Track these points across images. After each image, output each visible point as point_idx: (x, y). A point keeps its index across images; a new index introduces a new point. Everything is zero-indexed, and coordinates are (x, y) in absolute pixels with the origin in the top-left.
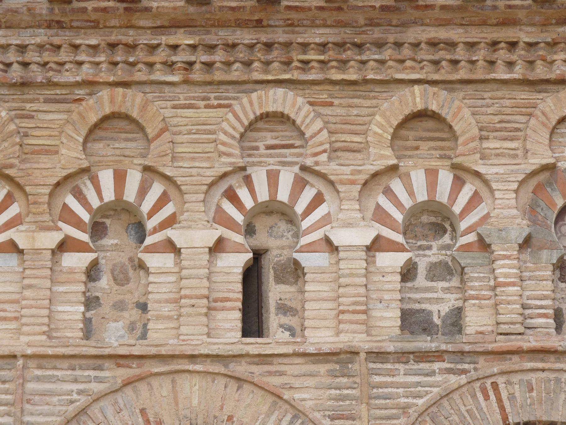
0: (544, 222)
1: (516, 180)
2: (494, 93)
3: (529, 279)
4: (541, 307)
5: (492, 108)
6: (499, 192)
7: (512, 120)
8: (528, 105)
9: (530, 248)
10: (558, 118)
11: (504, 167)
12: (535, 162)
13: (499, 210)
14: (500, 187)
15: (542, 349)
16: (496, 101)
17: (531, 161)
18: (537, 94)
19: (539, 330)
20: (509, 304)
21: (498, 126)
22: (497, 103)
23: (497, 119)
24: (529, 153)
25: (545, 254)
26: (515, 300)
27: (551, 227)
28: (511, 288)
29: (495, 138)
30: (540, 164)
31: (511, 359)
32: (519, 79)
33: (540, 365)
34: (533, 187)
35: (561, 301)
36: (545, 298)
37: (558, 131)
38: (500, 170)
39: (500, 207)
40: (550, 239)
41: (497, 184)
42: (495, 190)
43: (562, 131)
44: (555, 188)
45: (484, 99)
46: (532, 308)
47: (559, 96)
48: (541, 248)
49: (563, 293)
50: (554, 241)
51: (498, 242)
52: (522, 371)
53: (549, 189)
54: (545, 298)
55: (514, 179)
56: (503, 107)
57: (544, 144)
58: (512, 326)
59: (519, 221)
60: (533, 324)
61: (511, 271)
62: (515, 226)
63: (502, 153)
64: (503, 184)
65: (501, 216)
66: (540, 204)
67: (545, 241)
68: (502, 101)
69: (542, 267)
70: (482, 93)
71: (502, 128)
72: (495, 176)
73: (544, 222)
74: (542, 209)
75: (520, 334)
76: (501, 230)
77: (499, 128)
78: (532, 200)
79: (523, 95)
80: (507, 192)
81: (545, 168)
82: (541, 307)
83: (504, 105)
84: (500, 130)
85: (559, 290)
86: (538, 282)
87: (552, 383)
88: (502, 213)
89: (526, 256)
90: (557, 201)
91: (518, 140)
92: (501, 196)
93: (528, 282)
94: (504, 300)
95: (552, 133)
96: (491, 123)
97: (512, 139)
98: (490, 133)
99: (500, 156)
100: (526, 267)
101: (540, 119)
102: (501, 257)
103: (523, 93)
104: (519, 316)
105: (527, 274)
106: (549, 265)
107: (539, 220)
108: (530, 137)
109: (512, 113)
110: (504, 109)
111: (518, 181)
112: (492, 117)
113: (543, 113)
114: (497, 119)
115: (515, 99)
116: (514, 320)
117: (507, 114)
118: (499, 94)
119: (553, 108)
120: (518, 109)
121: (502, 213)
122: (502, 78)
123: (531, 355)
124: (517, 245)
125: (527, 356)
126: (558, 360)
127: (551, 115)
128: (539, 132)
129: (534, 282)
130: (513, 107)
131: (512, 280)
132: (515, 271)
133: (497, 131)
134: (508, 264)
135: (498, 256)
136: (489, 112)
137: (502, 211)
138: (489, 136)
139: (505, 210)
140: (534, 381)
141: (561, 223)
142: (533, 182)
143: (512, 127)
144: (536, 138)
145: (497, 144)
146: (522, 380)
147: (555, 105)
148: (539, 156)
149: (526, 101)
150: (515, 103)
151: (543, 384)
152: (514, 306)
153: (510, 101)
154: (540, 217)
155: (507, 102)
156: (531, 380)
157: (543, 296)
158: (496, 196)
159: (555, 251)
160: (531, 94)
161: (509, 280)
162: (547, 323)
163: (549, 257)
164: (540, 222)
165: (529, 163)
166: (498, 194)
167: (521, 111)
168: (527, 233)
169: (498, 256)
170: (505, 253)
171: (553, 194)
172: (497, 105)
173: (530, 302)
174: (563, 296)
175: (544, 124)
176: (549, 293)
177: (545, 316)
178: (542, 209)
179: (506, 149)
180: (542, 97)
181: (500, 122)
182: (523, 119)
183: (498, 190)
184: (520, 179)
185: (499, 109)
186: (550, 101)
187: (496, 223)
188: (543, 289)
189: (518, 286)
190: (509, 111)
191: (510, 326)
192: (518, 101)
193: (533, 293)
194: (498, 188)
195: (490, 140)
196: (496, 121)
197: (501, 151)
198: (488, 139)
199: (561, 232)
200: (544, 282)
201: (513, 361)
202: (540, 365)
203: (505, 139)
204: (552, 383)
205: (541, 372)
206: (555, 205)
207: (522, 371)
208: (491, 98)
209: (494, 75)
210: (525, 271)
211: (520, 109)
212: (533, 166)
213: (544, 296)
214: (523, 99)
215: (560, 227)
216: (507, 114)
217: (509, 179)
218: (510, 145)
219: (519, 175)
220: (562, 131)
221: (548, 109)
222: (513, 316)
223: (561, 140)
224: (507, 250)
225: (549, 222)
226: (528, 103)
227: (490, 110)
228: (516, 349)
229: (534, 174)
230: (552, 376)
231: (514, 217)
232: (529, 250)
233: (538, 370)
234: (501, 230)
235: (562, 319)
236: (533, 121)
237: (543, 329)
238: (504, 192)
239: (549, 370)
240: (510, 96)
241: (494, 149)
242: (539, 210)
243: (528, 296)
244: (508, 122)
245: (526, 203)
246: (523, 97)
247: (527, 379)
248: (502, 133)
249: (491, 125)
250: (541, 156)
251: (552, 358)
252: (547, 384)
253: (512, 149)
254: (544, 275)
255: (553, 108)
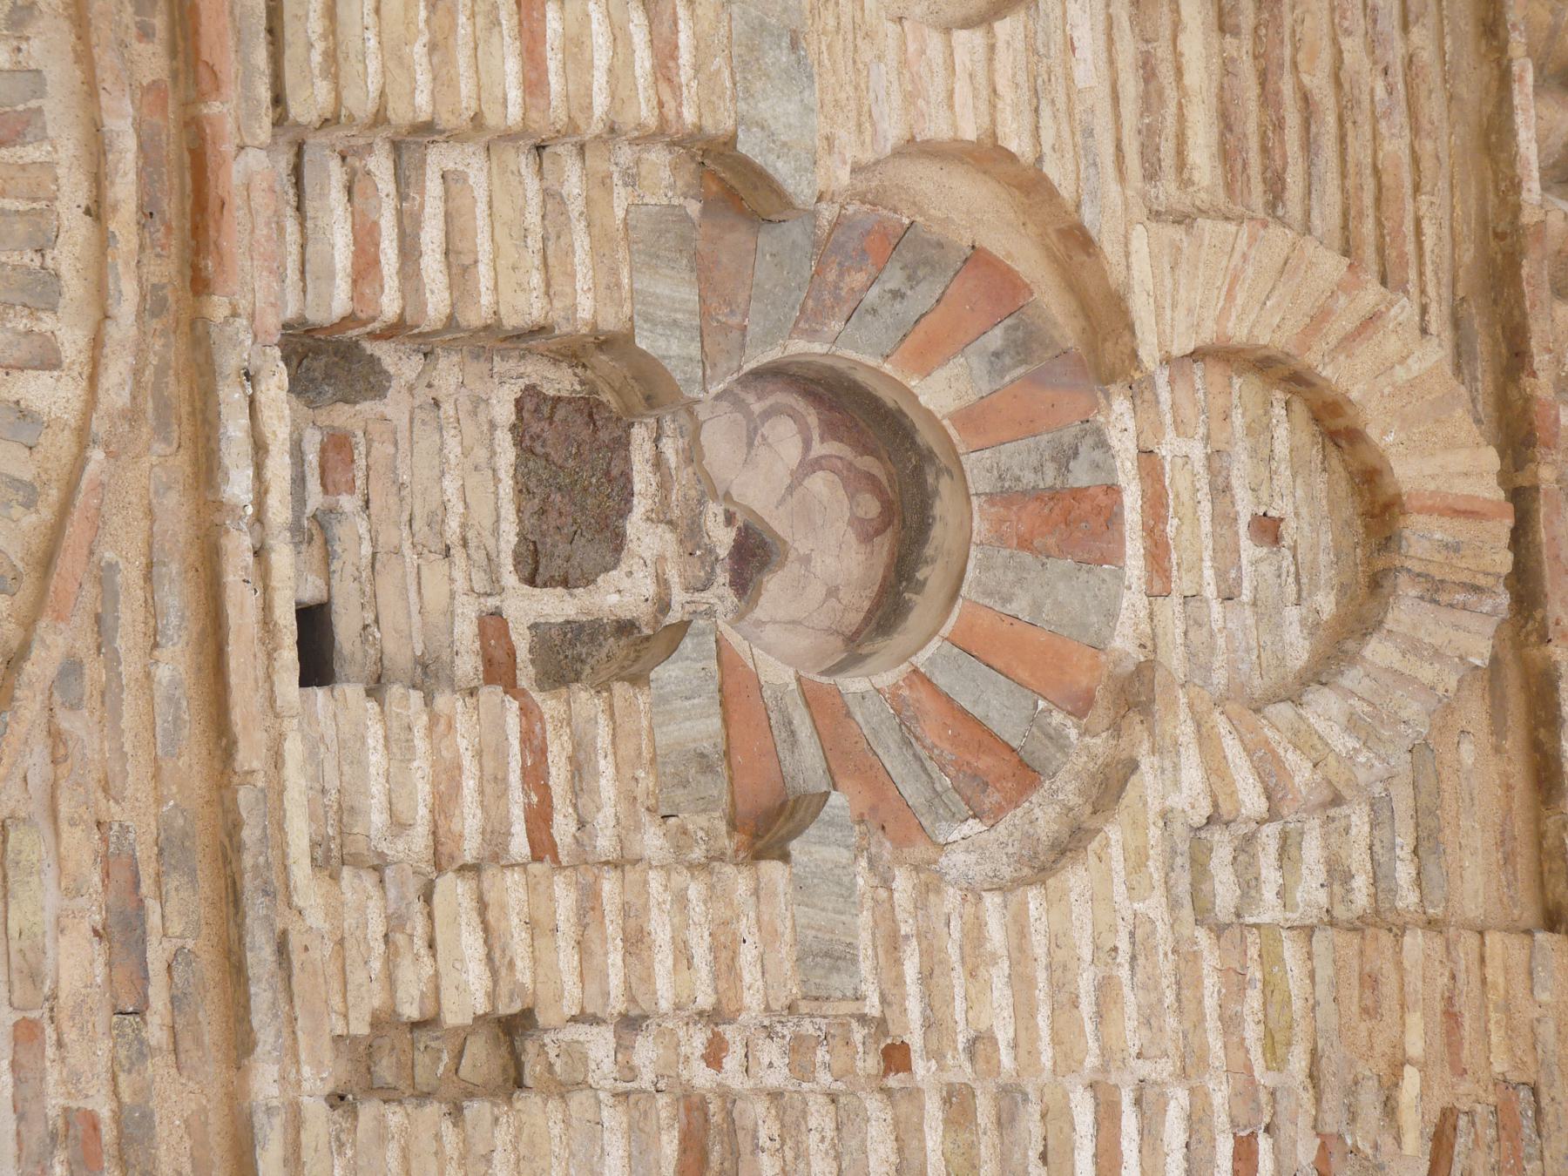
0: (838, 300)
1: (1046, 149)
2: (1434, 75)
3: (547, 194)
4: (409, 250)
5: (1367, 64)
6: (981, 52)
7: (1321, 163)
8: (1392, 254)
9: (704, 212)
10: (1354, 395)
11: (1104, 91)
12: (1137, 259)
13: (892, 43)
14: (1004, 59)
15: (213, 205)
16: (1400, 86)
17: (1140, 240)
18: (1446, 309)
19: (291, 227)
20: (432, 47)
21: (1287, 87)
22: (1390, 91)
23: (1318, 82)
24: (1177, 233)
25: (675, 291)
26: (453, 85)
27: (812, 334)
28: (512, 67)
29: (1228, 68)
30: (1128, 286)
31: (145, 33)
32: (1517, 209)
33: (124, 190)
34: (1000, 255)
35: (423, 395)
36: (459, 270)
37: (1279, 411)
38: (1087, 70)
39: (912, 47)
40: (753, 330)
41: (1019, 45)
42: (990, 32)
43: (1281, 433)
44: (1002, 372)
45: (1405, 27)
46: (402, 196)
47: (1459, 412)
48: (703, 270)
49: (466, 405)
50: (743, 347)
51: (739, 26)
52: (91, 89)
53: (995, 338)
54: (459, 270)
55: (1047, 136)
56: (1375, 121)
57: (1224, 314)
58: (316, 57)
59: (852, 149)
60: (323, 195)
61: (600, 79)
62: (820, 124)
63: (1160, 93)
64: (1022, 78)
65: (867, 53)
66: (924, 287)
67: (741, 298)
68: (1400, 117)
69: (614, 271)
70: (1431, 19)
71: (1279, 105)
72: (1058, 37)
73: (838, 300)
74: (897, 295)
75: (278, 100)
76: (794, 45)
77: (1278, 93)
78: (940, 245)
79: (1438, 225)
80: (985, 93)
81: (1106, 315)
82: (409, 250)
83: (1383, 125)
84: (1268, 97)
85: (478, 388)
86: (534, 243)
87: (30, 259)
88: (880, 58)
89: (663, 180)
90: (941, 375)
91: (1229, 187)
92: (961, 57)
93: (532, 186)
94: (453, 27)
95: (1265, 365)
96: (1296, 50)
97: (1227, 155)
98: (1247, 44)
99: (1147, 81)
100: (605, 182)
101: (1343, 300)
102: (665, 30)
103: (1446, 231)
104: (371, 107)
105: (573, 183)
106: (627, 309)
107: (841, 275)
108: (1253, 239)
109: (1351, 169)
110: (1367, 129)
111: (1040, 159)
112: (1326, 57)
113: (1371, 321)
114: (1318, 82)
115: (1417, 189)
116: (350, 69)
117: (1342, 139)
118: (1433, 108)
119: (1401, 374)
120: (1368, 199)
121: (880, 58)
122: (1519, 119)
123: (172, 146)
124: (729, 124)
125: (168, 124)
126: (152, 304)
127: (1365, 356)
128: (1280, 290)
129: (533, 218)
130: (1376, 172)
131: (555, 82)
132: (600, 102)
133: (1263, 78)
134: (629, 64)
135: (667, 17)
136: (1346, 43)
137: (892, 56)
138: (1236, 32)
139: (893, 76)
140: (32, 153)
141: (813, 419)
142: (1026, 257)
143: (1284, 156)
144: (1250, 270)
145: (1198, 76)
146: (39, 91)
147: (1412, 384)
148: (1168, 283)
149: (1410, 248)
150: (1400, 186)
151: (23, 206)
152: (423, 78)
153: (1406, 159)
154: (858, 279)
155: (1396, 146)
156: (42, 138)
157: (466, 260)
158: (961, 36)
159: (694, 350)
160: (1446, 278)
161: (553, 65)
162: (332, 276)
163: (661, 314)
164: (831, 276)
165: (1129, 224)
166: (968, 42)
167: (1361, 214)
168: (790, 186)
169: (667, 17)
170: (685, 57)
171: (974, 361)
172: (1380, 92)
173: (434, 187)
174: (448, 408)
175: (1320, 318)
176: (486, 299)
177: (365, 267)
178: (897, 295)
179: (1181, 118)
180: (1433, 328)
181: (1306, 98)
182: (1327, 216)
183: (992, 48)
184: (1051, 170)
185: (1366, 98)
186: (1428, 364)
187: (832, 23)
188: (502, 263)
189: (526, 108)
190: (1359, 150)
191: (320, 46)
192: (1410, 207)
193: (481, 208)
194: (1001, 45)
195: (1215, 37)
196: (1306, 79)
197: (1171, 94)
198: (1222, 29)
199: (767, 414)
200: (536, 279)
201: (138, 46)
202: (124, 190)
203: (1226, 120)
204: (30, 259)
205: (83, 197)
206: (925, 362)
207: (91, 89)
208: (1410, 60)
209: (1530, 78)
210: (586, 174)
211: (1370, 212)
212: (1119, 249)
213: (465, 269)
214: (1419, 232)
215: (793, 415)
216: (1342, 139)
217: (1046, 111)
218: (1201, 141)
219: (1070, 167)
220: (1281, 433)
221: (1392, 345)
222: (373, 65)
223: (1238, 419)
224: (697, 69)
225: (836, 325)
226: (1402, 255)
227: (1353, 47)
228: (205, 56)
229: (1075, 242)
230: (69, 258)
231: (864, 119)
232: (694, 208)
233: (99, 180)
234: (794, 45)
235: (329, 390)
236: (1331, 265)
237: (293, 250)
238: (981, 79)
239: (104, 241)
240: (1427, 164)
241: (1177, 54)
242: (894, 278)
243: (462, 177)
244: (1309, 145)
245: (921, 212)
246: (1429, 229)
247: (48, 116)
248: (1253, 106)
249: (1287, 52)
250: (1175, 290)
251: (165, 270)
252: (20, 228)
253: (1180, 153)
254: (572, 276)
255: (1401, 374)
